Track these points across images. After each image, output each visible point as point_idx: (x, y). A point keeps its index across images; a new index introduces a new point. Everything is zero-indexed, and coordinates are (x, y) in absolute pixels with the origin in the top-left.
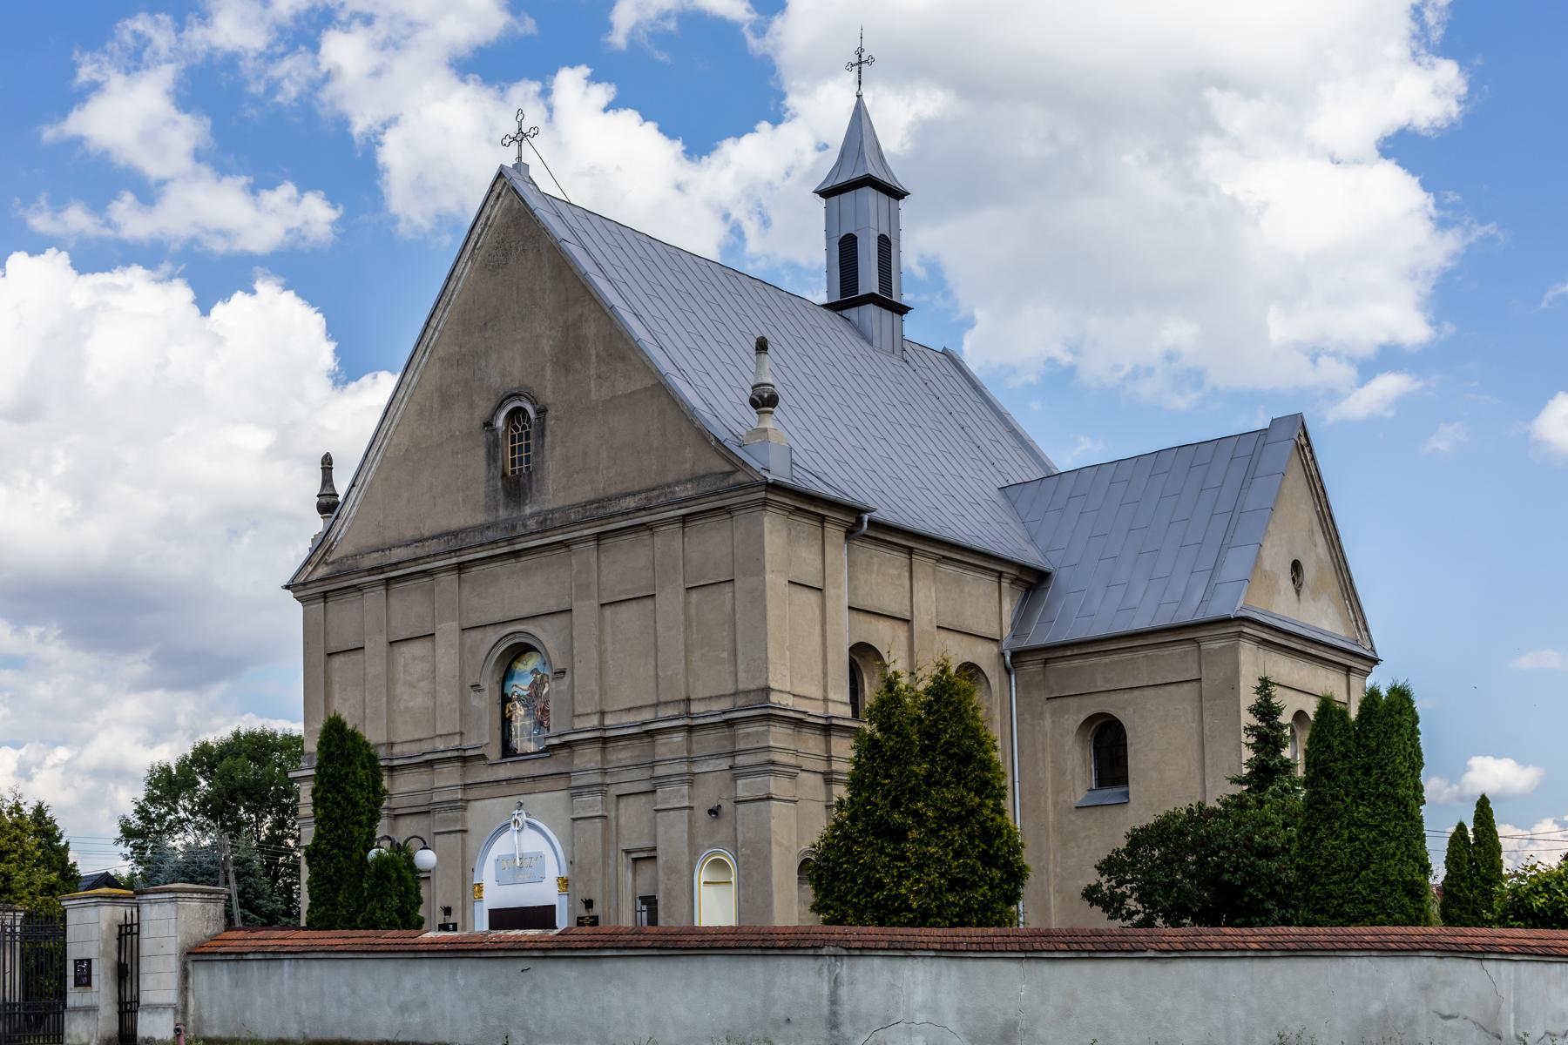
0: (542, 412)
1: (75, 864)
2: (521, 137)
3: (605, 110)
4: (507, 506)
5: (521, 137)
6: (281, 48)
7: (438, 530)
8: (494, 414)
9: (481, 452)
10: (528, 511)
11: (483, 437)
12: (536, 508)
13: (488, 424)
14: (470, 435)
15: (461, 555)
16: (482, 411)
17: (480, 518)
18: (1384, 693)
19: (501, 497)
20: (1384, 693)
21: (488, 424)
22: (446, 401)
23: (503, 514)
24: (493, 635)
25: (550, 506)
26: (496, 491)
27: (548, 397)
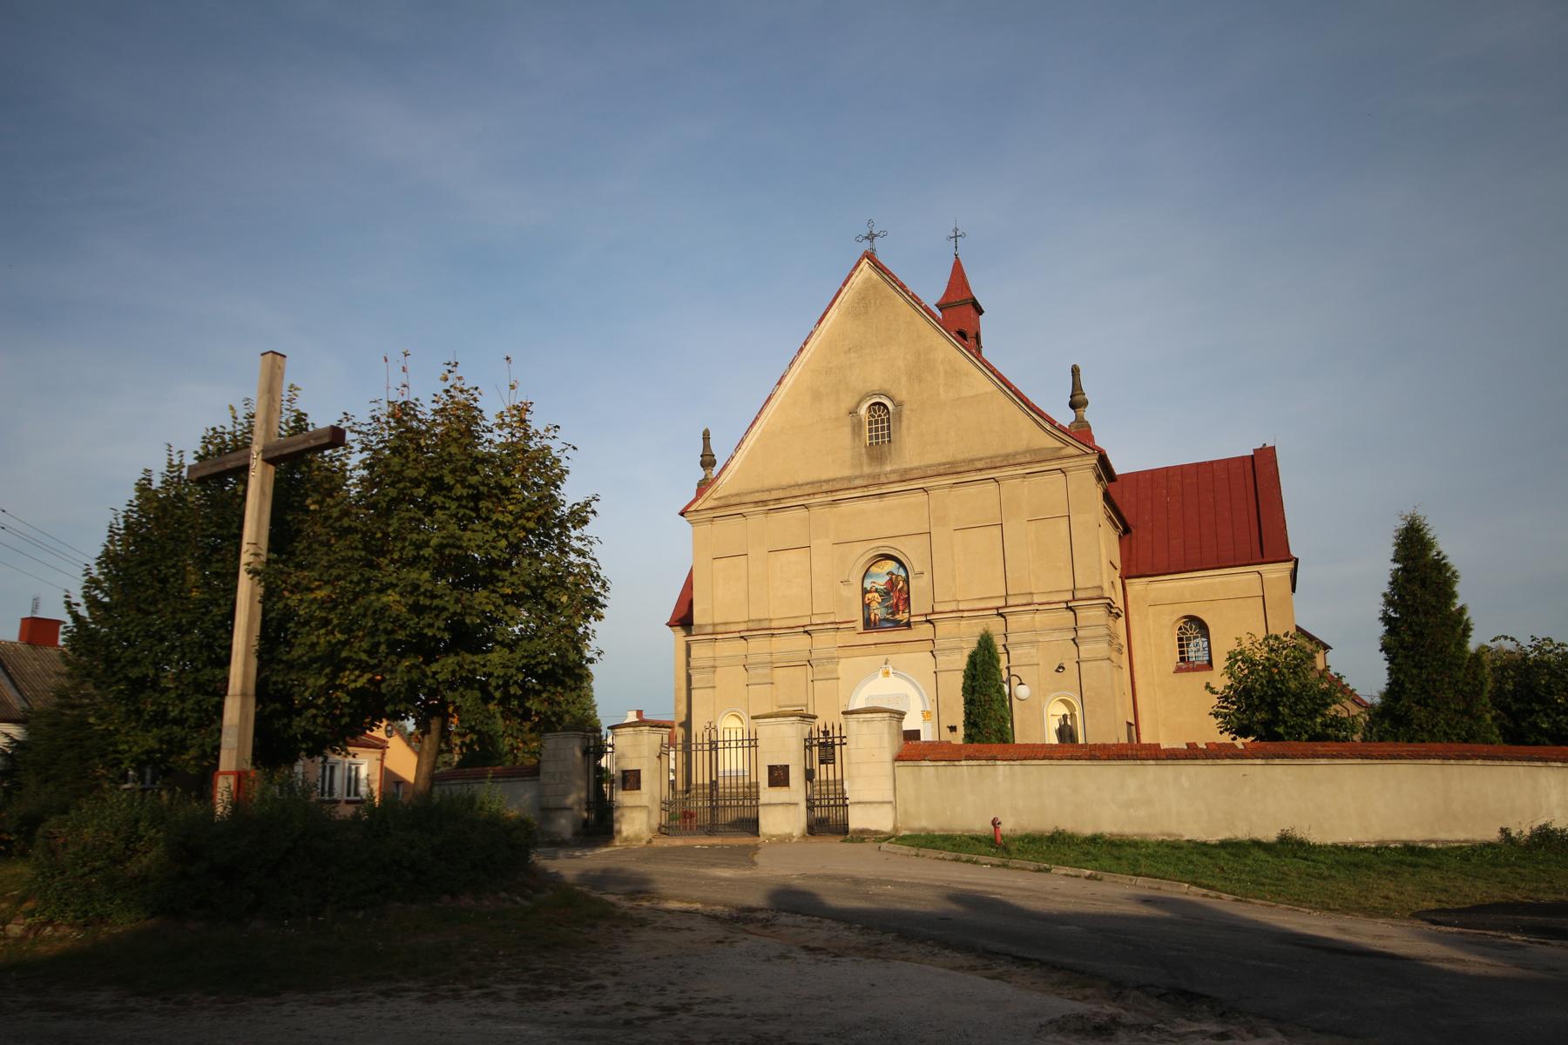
0: (898, 405)
1: (1462, 610)
2: (871, 237)
3: (1413, 546)
4: (870, 465)
5: (871, 237)
6: (1077, 398)
7: (810, 479)
8: (858, 405)
9: (847, 430)
10: (888, 468)
11: (848, 420)
12: (895, 467)
13: (853, 412)
14: (837, 419)
15: (832, 492)
16: (848, 403)
17: (847, 473)
18: (426, 410)
19: (865, 459)
20: (426, 410)
21: (853, 412)
22: (817, 396)
23: (867, 470)
24: (859, 548)
25: (908, 466)
26: (860, 455)
27: (902, 395)
